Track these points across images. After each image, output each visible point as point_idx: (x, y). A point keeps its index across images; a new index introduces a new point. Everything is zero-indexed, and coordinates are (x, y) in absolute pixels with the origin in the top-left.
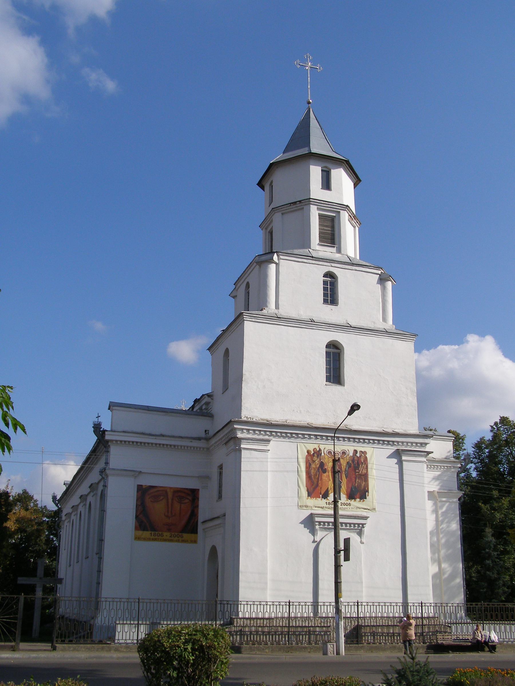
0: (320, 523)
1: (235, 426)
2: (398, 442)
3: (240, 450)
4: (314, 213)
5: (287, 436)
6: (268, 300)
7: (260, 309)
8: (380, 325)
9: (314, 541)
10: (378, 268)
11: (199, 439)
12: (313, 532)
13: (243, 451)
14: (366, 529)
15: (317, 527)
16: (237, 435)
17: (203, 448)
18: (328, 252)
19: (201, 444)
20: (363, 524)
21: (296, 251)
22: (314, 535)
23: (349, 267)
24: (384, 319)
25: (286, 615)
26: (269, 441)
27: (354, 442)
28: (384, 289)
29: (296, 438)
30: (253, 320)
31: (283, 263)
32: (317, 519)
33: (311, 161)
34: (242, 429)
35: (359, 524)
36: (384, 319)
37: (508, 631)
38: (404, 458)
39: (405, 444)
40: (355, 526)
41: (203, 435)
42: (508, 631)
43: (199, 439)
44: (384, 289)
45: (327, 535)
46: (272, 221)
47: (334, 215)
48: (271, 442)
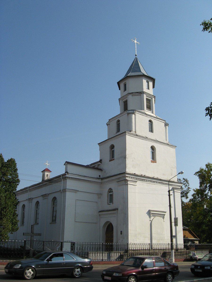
0: (152, 213)
1: (126, 175)
2: (173, 185)
3: (127, 184)
4: (145, 97)
5: (141, 180)
6: (133, 128)
7: (130, 131)
8: (165, 142)
9: (150, 221)
10: (165, 121)
11: (97, 178)
12: (150, 217)
13: (129, 185)
14: (165, 216)
15: (151, 215)
16: (126, 178)
17: (100, 183)
18: (149, 113)
19: (99, 181)
20: (165, 215)
21: (140, 111)
22: (150, 218)
23: (156, 119)
24: (166, 140)
25: (168, 248)
26: (137, 182)
27: (161, 184)
28: (166, 128)
29: (144, 181)
30: (129, 135)
31: (136, 114)
32: (152, 212)
33: (143, 78)
34: (128, 177)
35: (163, 214)
36: (166, 140)
37: (115, 256)
38: (175, 191)
39: (175, 185)
40: (162, 215)
41: (98, 177)
42: (115, 256)
43: (97, 178)
44: (166, 128)
45: (153, 218)
46: (127, 97)
47: (151, 99)
48: (137, 182)
